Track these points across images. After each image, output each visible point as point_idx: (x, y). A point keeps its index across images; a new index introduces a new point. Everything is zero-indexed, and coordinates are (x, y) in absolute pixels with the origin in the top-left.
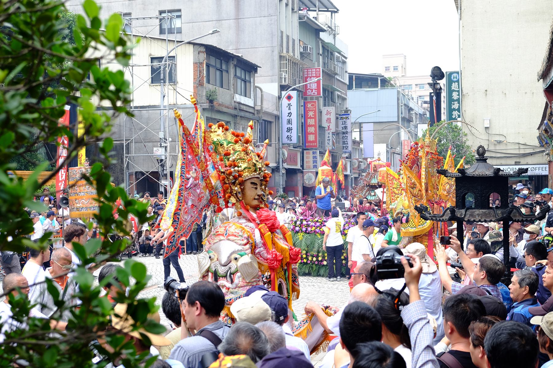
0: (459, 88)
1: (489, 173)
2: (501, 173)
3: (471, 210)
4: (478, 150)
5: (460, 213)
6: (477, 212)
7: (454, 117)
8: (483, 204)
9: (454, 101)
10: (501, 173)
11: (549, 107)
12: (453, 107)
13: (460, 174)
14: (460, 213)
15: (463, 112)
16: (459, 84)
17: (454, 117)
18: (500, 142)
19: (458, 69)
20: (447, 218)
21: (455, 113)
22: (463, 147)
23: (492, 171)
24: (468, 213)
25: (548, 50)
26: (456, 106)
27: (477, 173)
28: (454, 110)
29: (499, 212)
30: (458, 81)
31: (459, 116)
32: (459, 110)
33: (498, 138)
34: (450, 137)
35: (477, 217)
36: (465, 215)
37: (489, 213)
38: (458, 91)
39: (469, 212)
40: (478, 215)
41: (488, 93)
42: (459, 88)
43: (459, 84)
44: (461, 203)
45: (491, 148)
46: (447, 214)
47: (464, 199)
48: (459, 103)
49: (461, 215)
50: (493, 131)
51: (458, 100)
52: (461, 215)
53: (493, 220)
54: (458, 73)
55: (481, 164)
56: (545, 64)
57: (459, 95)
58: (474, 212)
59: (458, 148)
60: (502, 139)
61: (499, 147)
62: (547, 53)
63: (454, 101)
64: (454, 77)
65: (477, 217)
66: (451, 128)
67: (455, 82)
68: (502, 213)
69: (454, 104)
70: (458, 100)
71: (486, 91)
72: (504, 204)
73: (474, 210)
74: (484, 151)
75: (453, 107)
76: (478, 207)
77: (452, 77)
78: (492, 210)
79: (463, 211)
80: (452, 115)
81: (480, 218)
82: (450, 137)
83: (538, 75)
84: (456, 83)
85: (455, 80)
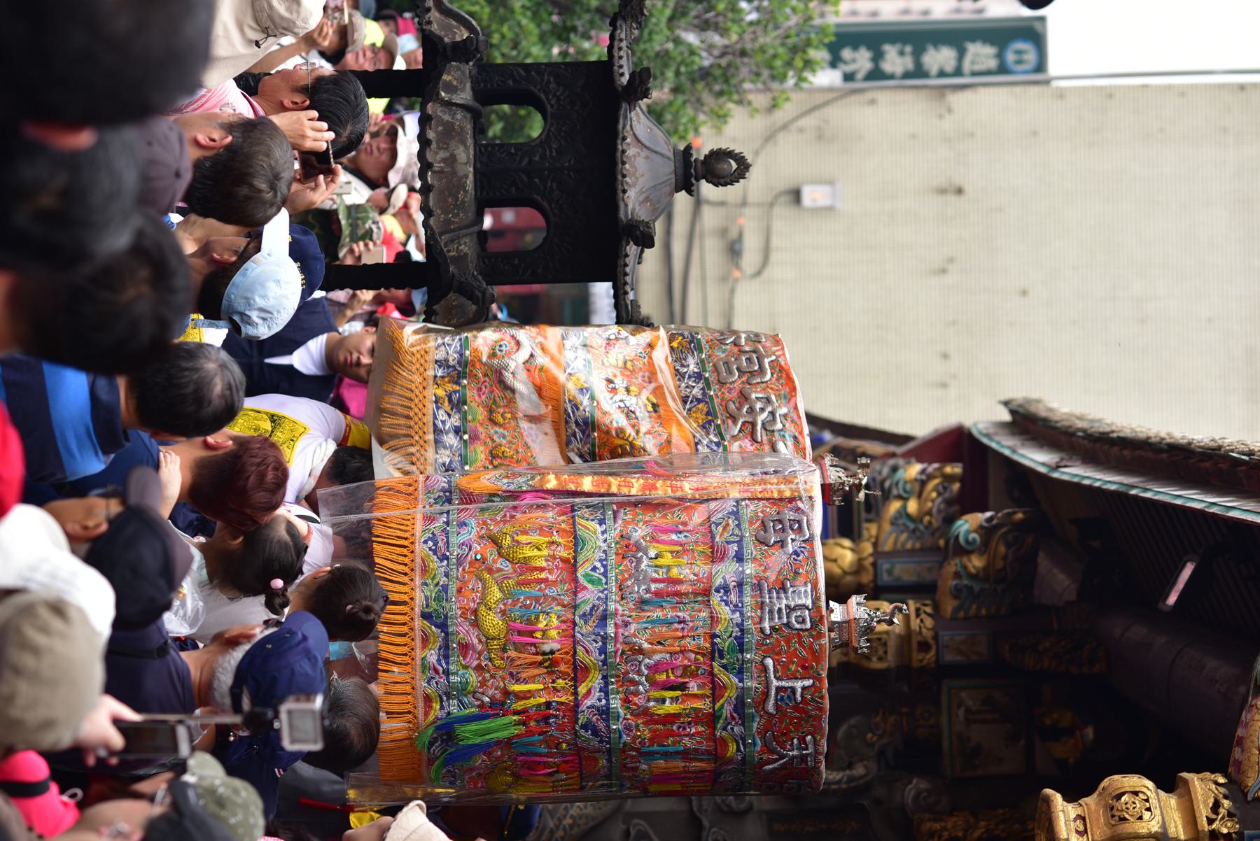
0: (974, 74)
1: (633, 202)
2: (632, 249)
3: (469, 127)
4: (730, 154)
5: (458, 85)
6: (464, 155)
7: (846, 53)
8: (500, 178)
9: (918, 54)
10: (632, 249)
11: (892, 448)
12: (891, 51)
13: (625, 80)
14: (458, 85)
15: (869, 95)
16: (989, 73)
17: (846, 53)
18: (734, 251)
19: (1056, 64)
20: (435, 27)
21: (861, 60)
22: (720, 94)
23: (642, 214)
24: (459, 115)
25: (1142, 436)
26: (895, 61)
27: (631, 152)
28: (878, 56)
29: (467, 247)
30: (1003, 69)
31: (848, 77)
32: (876, 74)
33: (751, 245)
34: (769, 39)
35: (442, 154)
36: (449, 104)
37: (460, 206)
38: (958, 72)
39: (462, 120)
40: (451, 160)
41: (951, 198)
42: (974, 74)
43: (989, 73)
44: (505, 85)
45: (710, 218)
46: (449, 29)
47: (521, 98)
48: (907, 75)
49: (450, 88)
50: (783, 217)
51: (919, 72)
52: (450, 88)
53: (432, 221)
54: (1041, 67)
55: (667, 170)
56: (1080, 424)
57: (942, 74)
58: (464, 143)
59: (718, 72)
60: (750, 258)
61: (711, 252)
62: (1127, 433)
63: (918, 54)
64: (1019, 52)
65: (442, 154)
66: (808, 43)
67: (1000, 56)
68: (461, 259)
69: (902, 53)
70: (919, 72)
71: (960, 191)
72: (502, 263)
73: (470, 142)
74: (720, 180)
75: (891, 51)
76: (486, 156)
77: (1020, 45)
78: (471, 215)
79: (465, 96)
80: (855, 47)
81: (437, 166)
82: (769, 39)
83: (1028, 401)
84: (993, 64)
85: (1010, 57)
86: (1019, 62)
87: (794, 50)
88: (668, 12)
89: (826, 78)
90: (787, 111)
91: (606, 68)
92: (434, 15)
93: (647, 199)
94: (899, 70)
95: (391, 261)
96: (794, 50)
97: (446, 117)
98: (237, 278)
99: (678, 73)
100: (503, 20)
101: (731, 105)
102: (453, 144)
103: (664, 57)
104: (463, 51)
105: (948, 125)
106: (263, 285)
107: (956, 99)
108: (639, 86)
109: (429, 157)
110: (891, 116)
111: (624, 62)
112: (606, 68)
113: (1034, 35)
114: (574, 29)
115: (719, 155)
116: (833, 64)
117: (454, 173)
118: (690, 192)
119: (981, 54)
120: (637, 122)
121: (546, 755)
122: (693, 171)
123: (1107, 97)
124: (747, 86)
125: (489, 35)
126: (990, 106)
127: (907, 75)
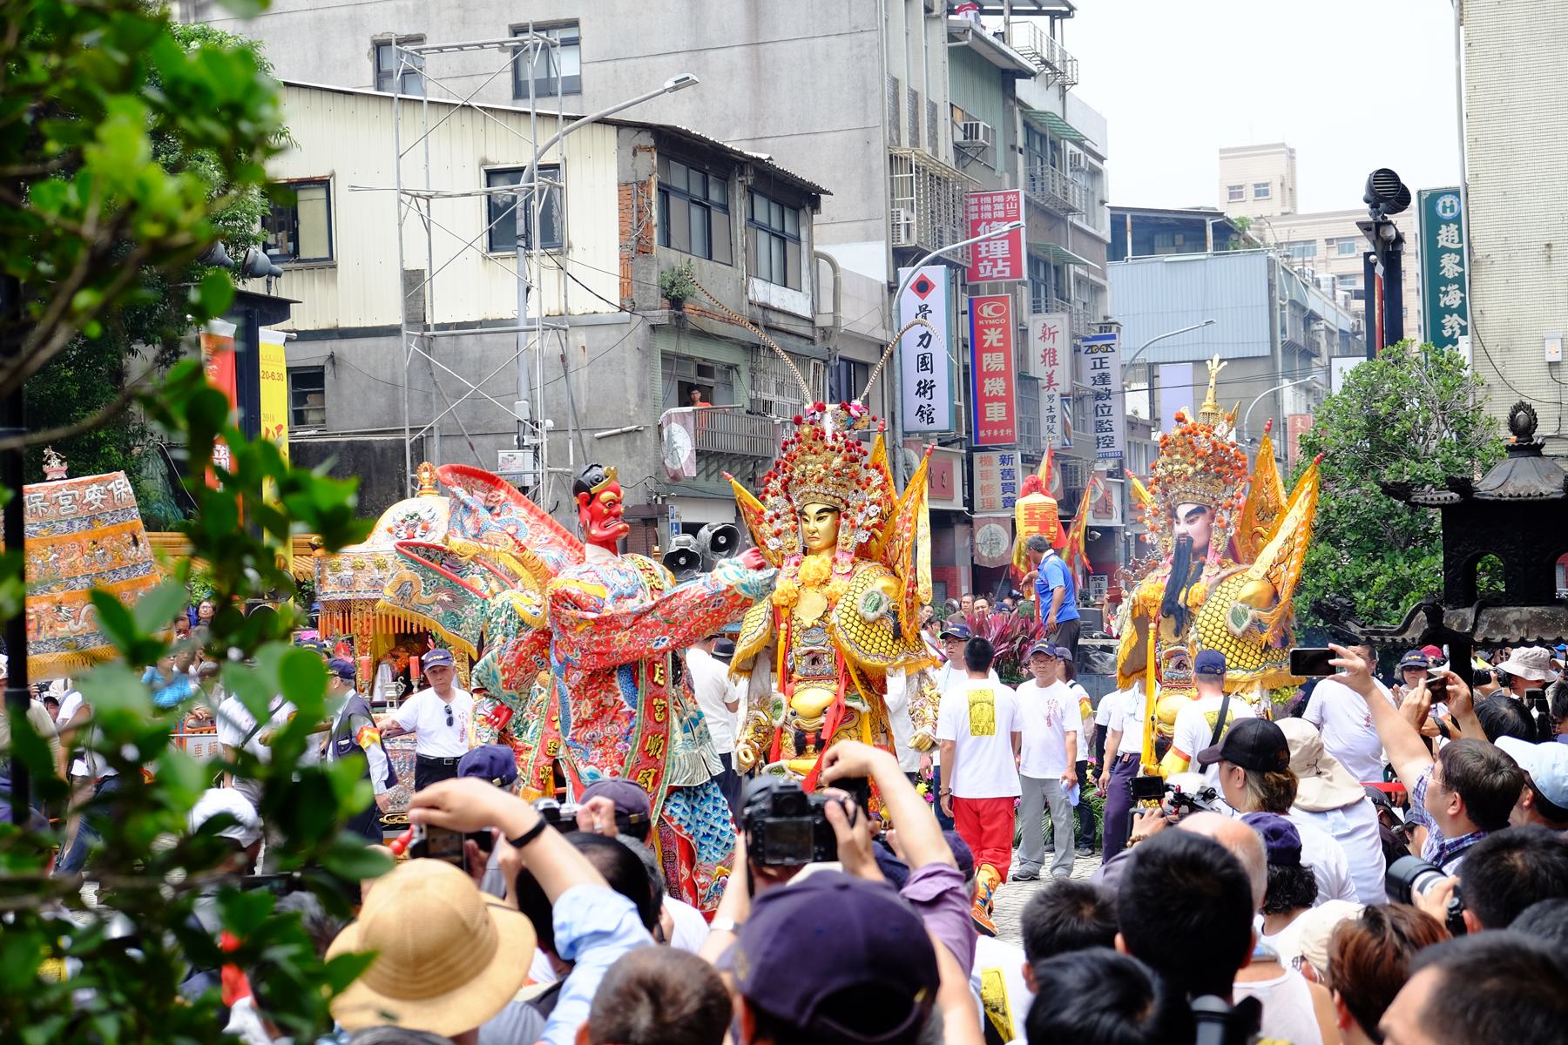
0: (1461, 241)
4: (1512, 417)
5: (1460, 618)
6: (1513, 614)
7: (1447, 333)
13: (1455, 496)
14: (1460, 618)
15: (1477, 315)
16: (1460, 229)
19: (1455, 182)
20: (1417, 635)
21: (1451, 322)
26: (1452, 298)
27: (1511, 490)
28: (1449, 310)
30: (1457, 220)
31: (1464, 331)
34: (1432, 389)
36: (1475, 625)
37: (1554, 618)
38: (1459, 252)
40: (1518, 623)
43: (1460, 229)
47: (1472, 575)
48: (1462, 289)
49: (1463, 624)
52: (1463, 624)
54: (1455, 193)
55: (1525, 463)
64: (1444, 208)
65: (1514, 629)
67: (1447, 222)
69: (1446, 293)
70: (1459, 280)
71: (1549, 246)
73: (1504, 610)
77: (1440, 209)
79: (1469, 613)
84: (1453, 227)
85: (1448, 215)
86: (1452, 207)
87: (1440, 370)
88: (1413, 463)
89: (1464, 347)
90: (1489, 376)
91: (1447, 509)
92: (1408, 636)
93: (1548, 477)
94: (1459, 294)
95: (309, 737)
96: (1440, 370)
97: (1485, 627)
98: (1547, 795)
99: (1459, 455)
100: (1419, 582)
101: (1482, 416)
102: (1506, 622)
103: (1447, 465)
104: (1434, 614)
105: (1498, 258)
106: (1556, 778)
107: (1479, 252)
108: (1463, 486)
109: (1515, 640)
110: (1494, 300)
111: (1442, 497)
112: (1447, 509)
113: (1431, 199)
114: (1426, 530)
115: (1513, 425)
116: (1455, 342)
117: (1528, 621)
118: (1542, 445)
119: (1446, 236)
120: (1488, 485)
121: (532, 401)
122: (1525, 441)
123: (1471, 141)
124: (1470, 403)
125: (1432, 593)
126: (1484, 229)
127: (1462, 289)
